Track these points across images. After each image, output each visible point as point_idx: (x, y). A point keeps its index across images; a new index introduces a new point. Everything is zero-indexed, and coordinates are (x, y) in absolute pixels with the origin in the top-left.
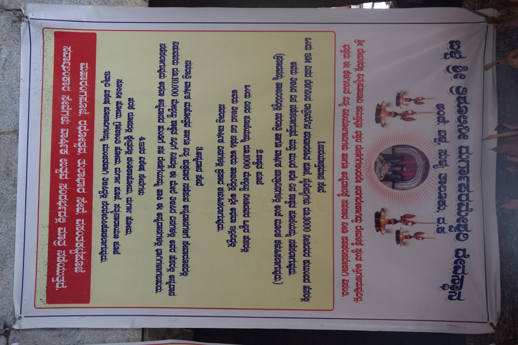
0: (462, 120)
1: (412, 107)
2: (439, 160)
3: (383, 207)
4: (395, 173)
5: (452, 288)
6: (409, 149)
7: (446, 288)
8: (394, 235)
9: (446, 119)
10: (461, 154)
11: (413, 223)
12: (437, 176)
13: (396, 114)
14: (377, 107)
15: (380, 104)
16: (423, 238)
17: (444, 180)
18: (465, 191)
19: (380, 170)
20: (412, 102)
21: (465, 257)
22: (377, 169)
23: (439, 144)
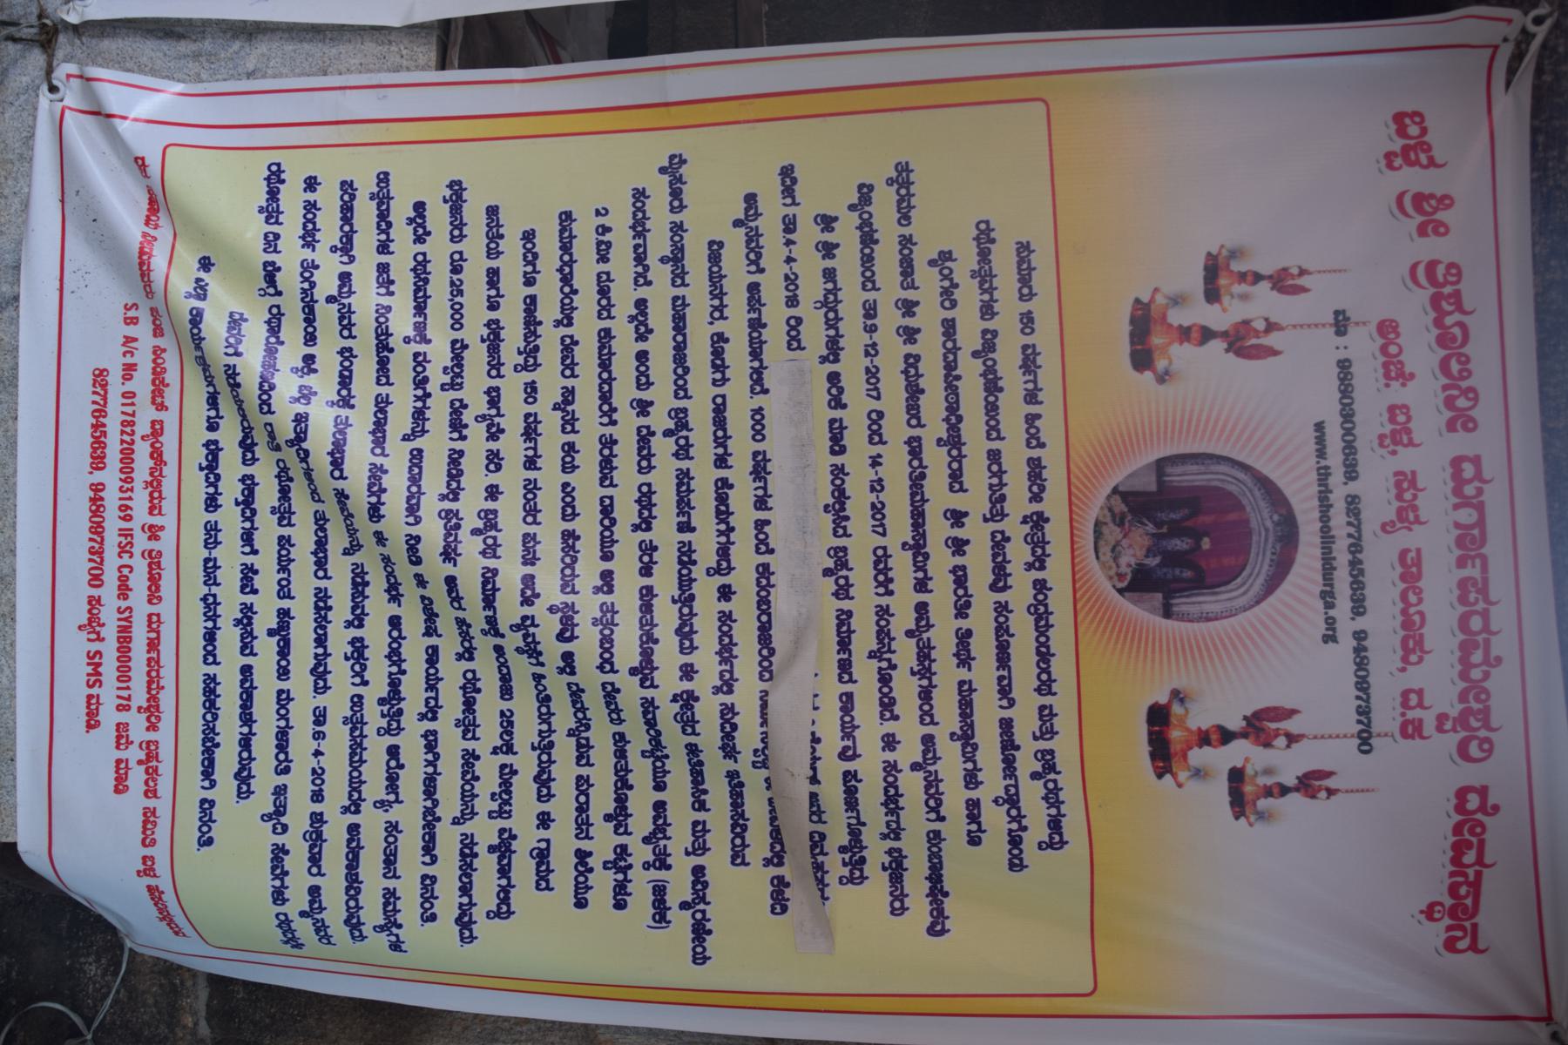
0: (1455, 367)
1: (1262, 303)
2: (1396, 504)
3: (1176, 684)
4: (1171, 559)
5: (1452, 912)
6: (1214, 468)
7: (1437, 916)
8: (1219, 789)
9: (1407, 370)
10: (1459, 481)
11: (1292, 739)
12: (1395, 559)
13: (1206, 335)
14: (1134, 309)
15: (1145, 299)
16: (1331, 792)
17: (1414, 569)
18: (1477, 600)
19: (1115, 550)
20: (1264, 286)
21: (1487, 814)
22: (1105, 550)
23: (1394, 453)
